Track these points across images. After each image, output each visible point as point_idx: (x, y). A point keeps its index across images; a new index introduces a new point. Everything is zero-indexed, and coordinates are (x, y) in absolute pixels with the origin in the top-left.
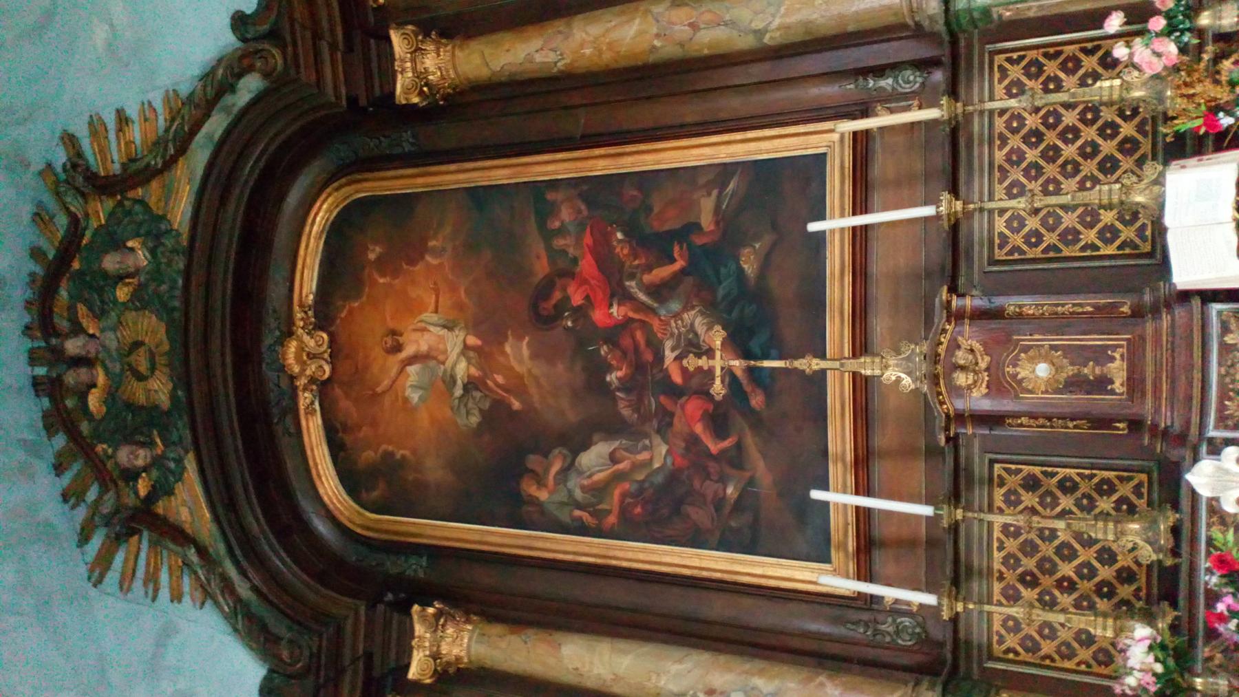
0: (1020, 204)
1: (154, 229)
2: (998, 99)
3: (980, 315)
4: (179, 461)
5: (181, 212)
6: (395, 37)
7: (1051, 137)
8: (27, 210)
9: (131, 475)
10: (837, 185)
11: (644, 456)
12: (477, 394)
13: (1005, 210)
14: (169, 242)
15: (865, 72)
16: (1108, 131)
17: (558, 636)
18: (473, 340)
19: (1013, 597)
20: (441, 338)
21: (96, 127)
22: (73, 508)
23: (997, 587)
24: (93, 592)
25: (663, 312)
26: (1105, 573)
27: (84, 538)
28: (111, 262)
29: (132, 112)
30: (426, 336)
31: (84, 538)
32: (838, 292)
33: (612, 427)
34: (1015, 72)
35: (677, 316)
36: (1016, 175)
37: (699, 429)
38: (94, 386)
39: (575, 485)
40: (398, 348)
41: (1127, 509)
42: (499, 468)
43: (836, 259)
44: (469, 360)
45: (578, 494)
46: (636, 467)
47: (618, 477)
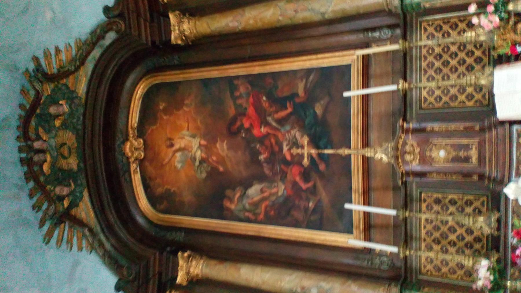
0: (433, 84)
1: (71, 96)
2: (424, 41)
3: (415, 131)
4: (81, 193)
5: (82, 89)
6: (171, 16)
7: (446, 57)
8: (18, 88)
9: (61, 199)
10: (356, 77)
11: (274, 190)
12: (205, 165)
13: (427, 87)
14: (77, 101)
15: (367, 30)
16: (470, 53)
17: (239, 265)
18: (203, 142)
19: (430, 248)
20: (190, 142)
21: (47, 54)
22: (37, 212)
23: (423, 245)
24: (45, 247)
25: (283, 131)
26: (469, 238)
27: (42, 224)
28: (53, 110)
29: (62, 47)
30: (184, 140)
31: (42, 224)
32: (356, 122)
33: (261, 178)
34: (431, 30)
35: (289, 132)
36: (431, 72)
37: (298, 179)
38: (45, 161)
39: (246, 202)
40: (172, 145)
41: (478, 212)
42: (214, 197)
43: (355, 108)
44: (201, 151)
45: (247, 206)
46: (271, 195)
47: (264, 199)
